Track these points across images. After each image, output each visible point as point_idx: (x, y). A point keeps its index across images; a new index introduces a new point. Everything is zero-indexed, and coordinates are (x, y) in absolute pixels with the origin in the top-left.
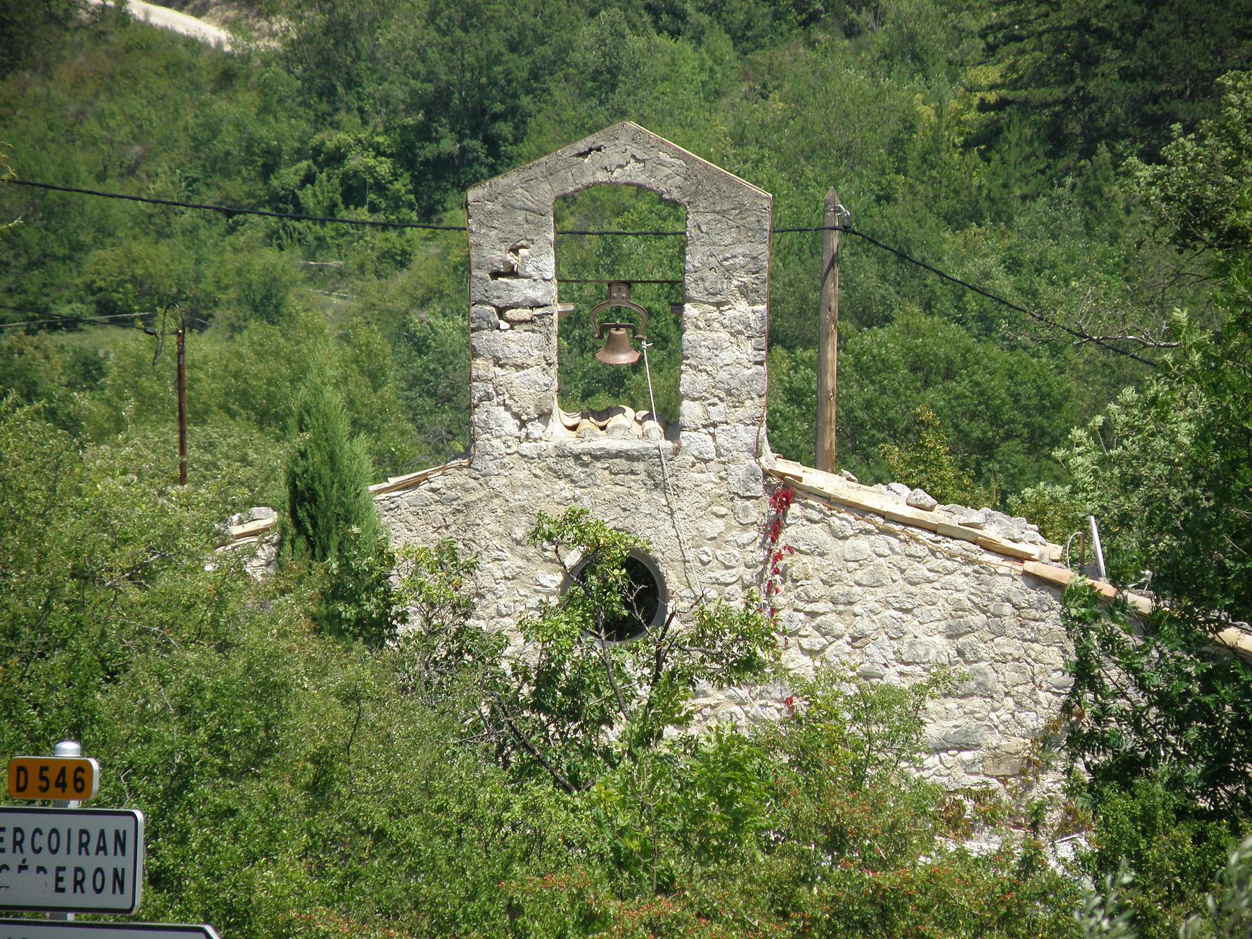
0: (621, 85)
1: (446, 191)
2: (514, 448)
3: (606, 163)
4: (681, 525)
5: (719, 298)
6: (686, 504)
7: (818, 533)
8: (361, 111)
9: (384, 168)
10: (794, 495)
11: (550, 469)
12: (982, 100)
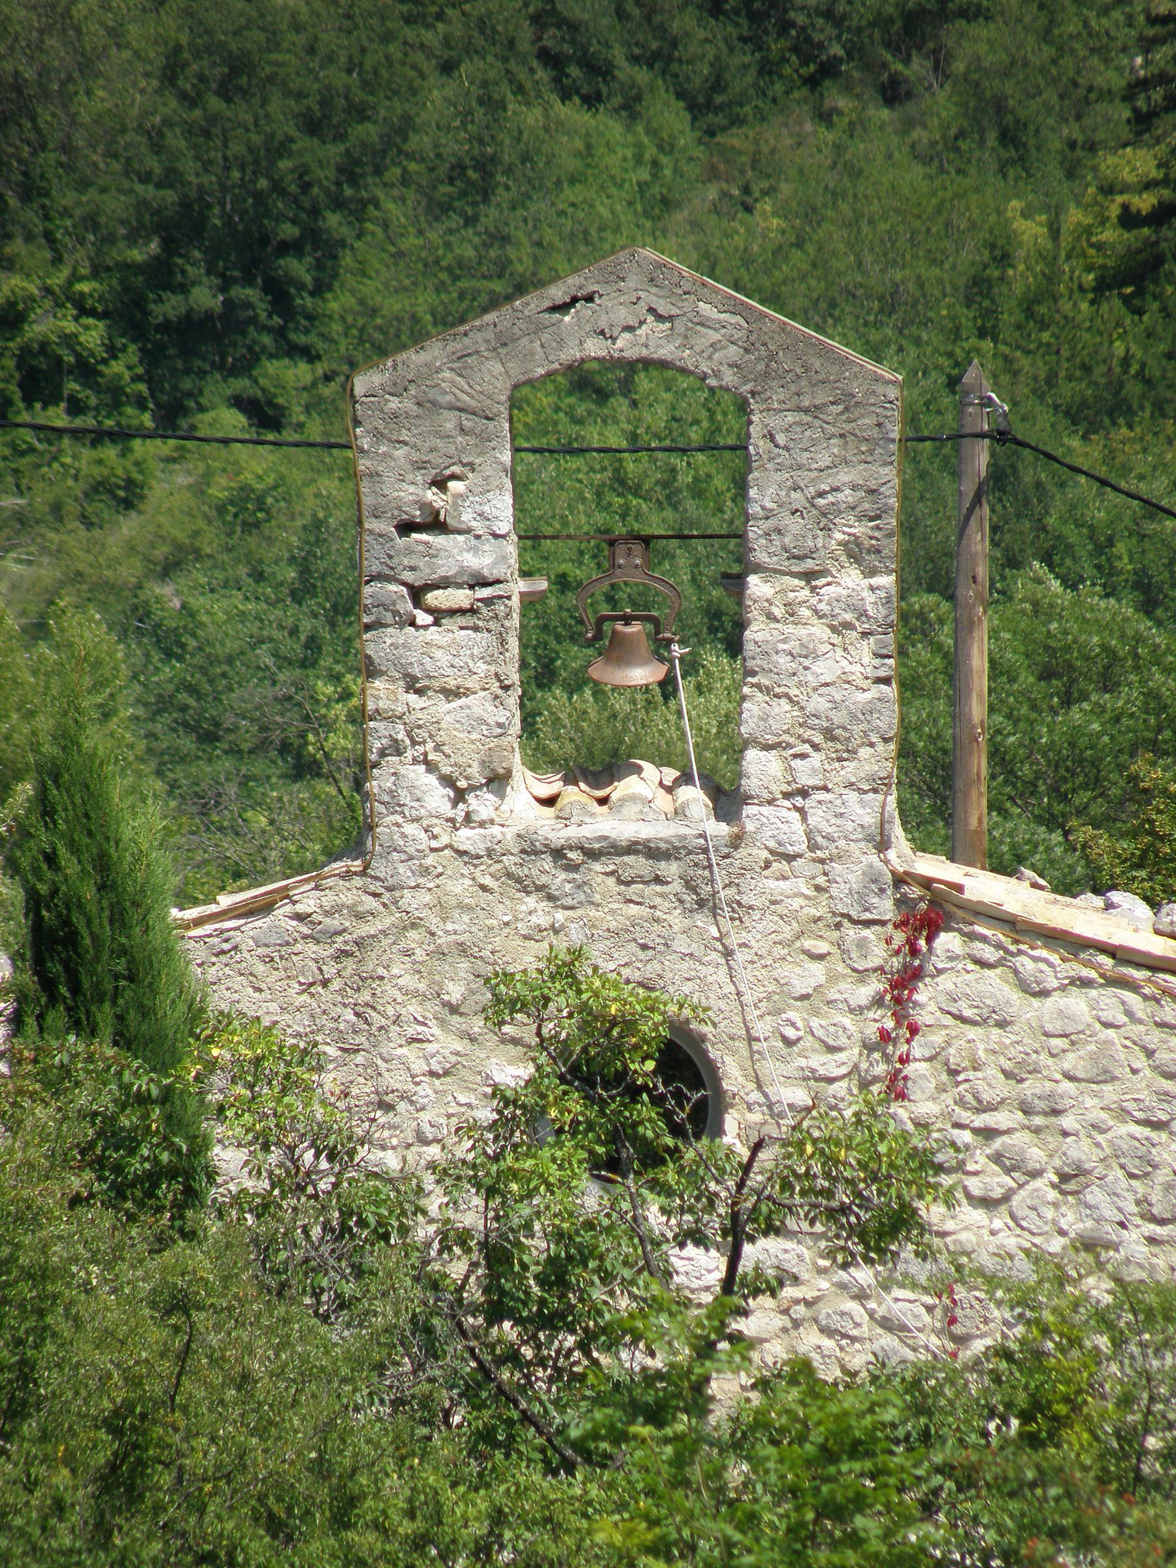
0: (500, 190)
1: (202, 374)
2: (445, 840)
3: (603, 323)
4: (745, 975)
5: (809, 564)
6: (756, 934)
7: (995, 986)
8: (49, 236)
9: (93, 336)
10: (950, 916)
11: (509, 875)
12: (1125, 207)
